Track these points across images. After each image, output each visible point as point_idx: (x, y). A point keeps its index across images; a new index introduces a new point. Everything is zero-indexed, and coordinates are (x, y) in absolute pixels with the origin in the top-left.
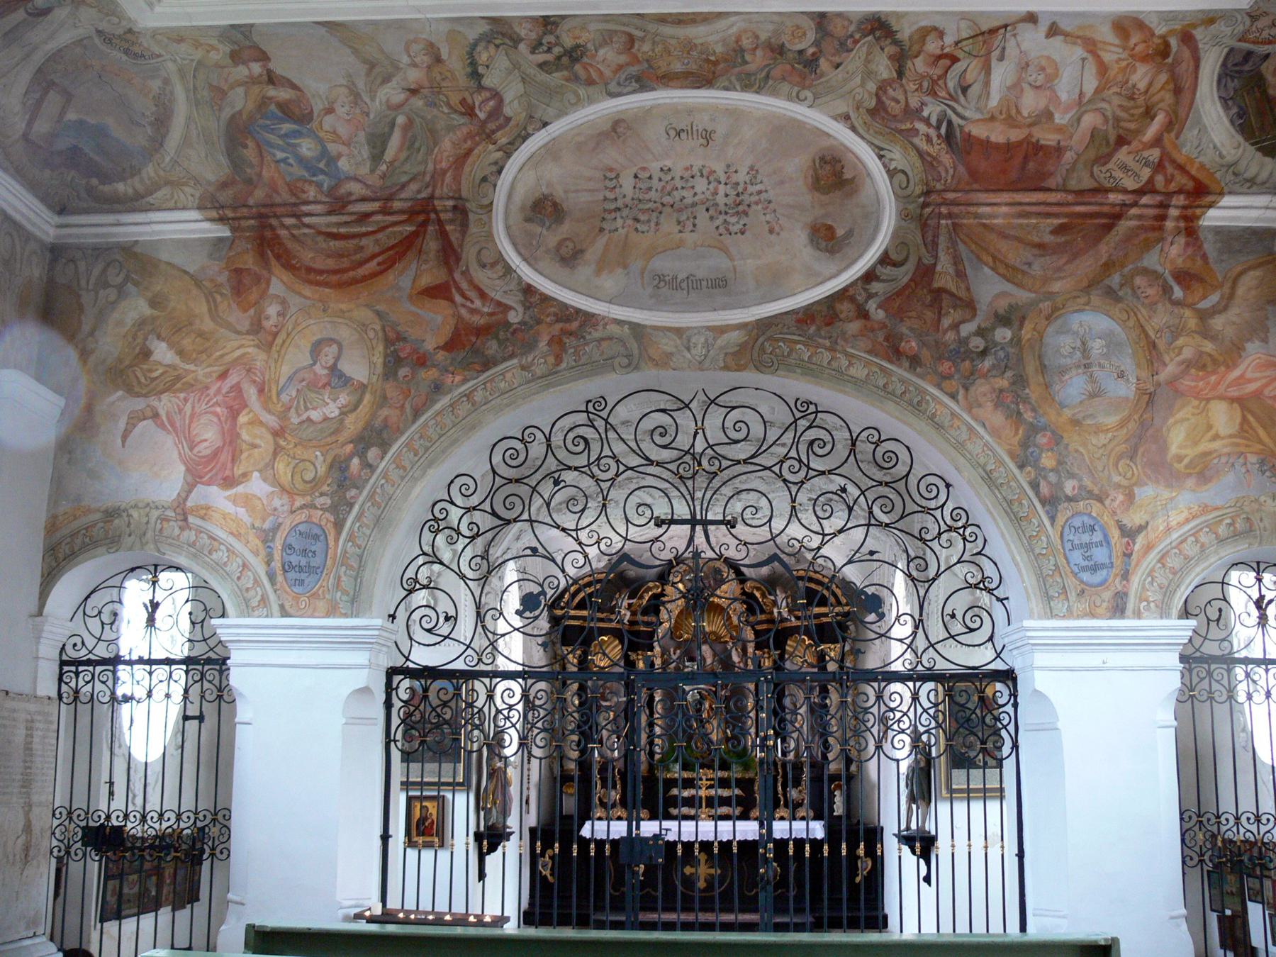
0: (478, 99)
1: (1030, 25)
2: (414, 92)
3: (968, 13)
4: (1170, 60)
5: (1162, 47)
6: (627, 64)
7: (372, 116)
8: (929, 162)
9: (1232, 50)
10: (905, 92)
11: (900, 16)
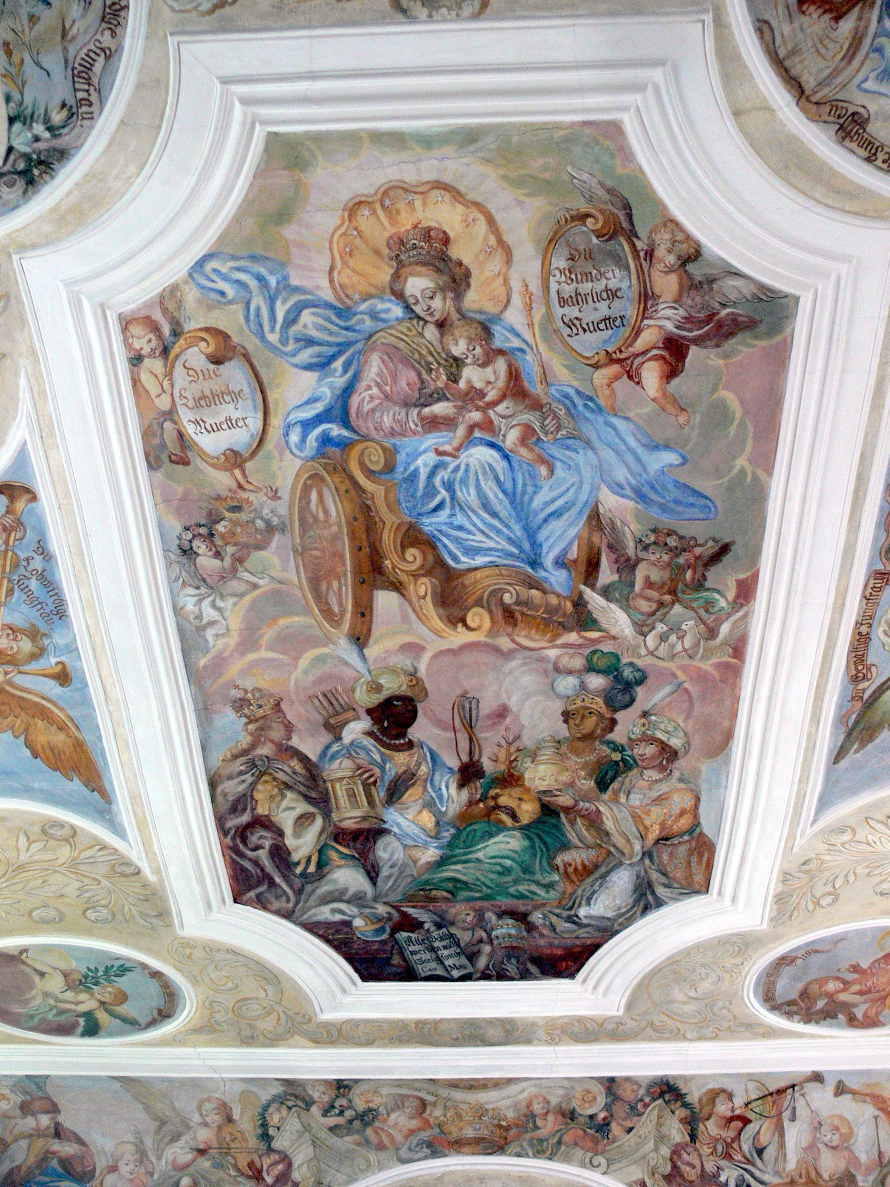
0: (267, 1162)
1: (818, 1085)
2: (202, 1152)
3: (753, 1074)
6: (420, 1129)
7: (156, 1177)
10: (700, 1156)
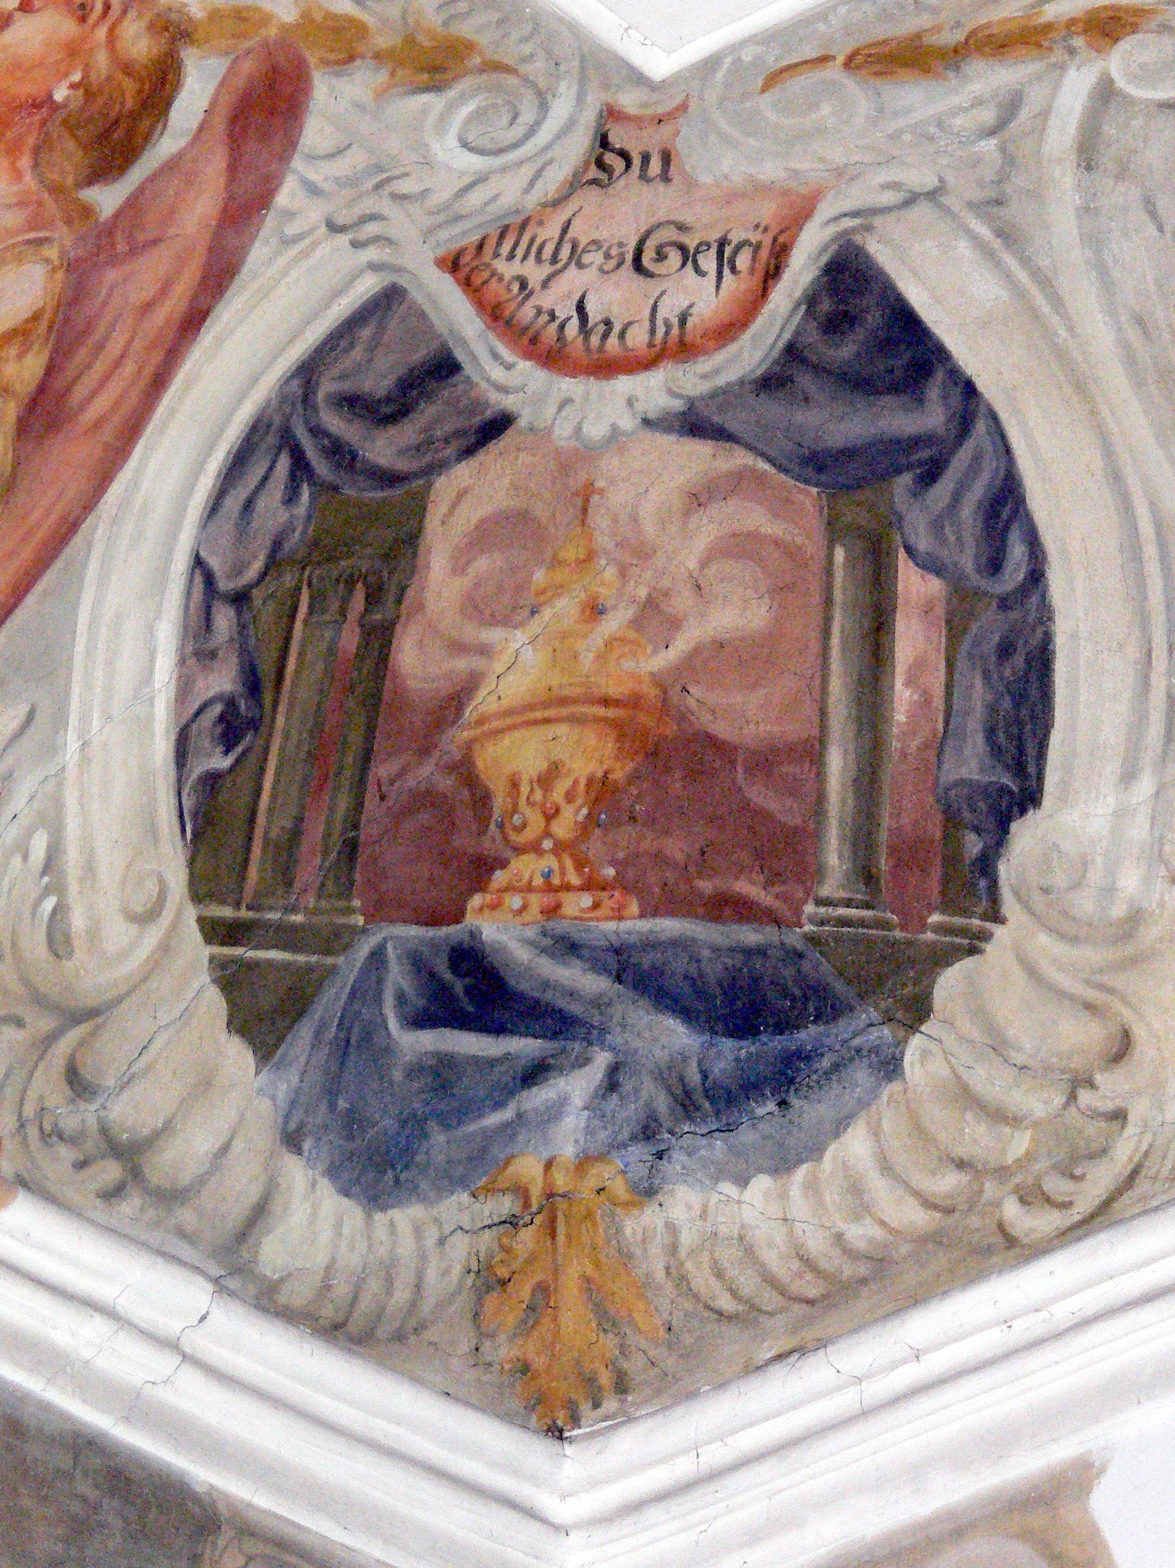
4: (107, 199)
9: (390, 298)
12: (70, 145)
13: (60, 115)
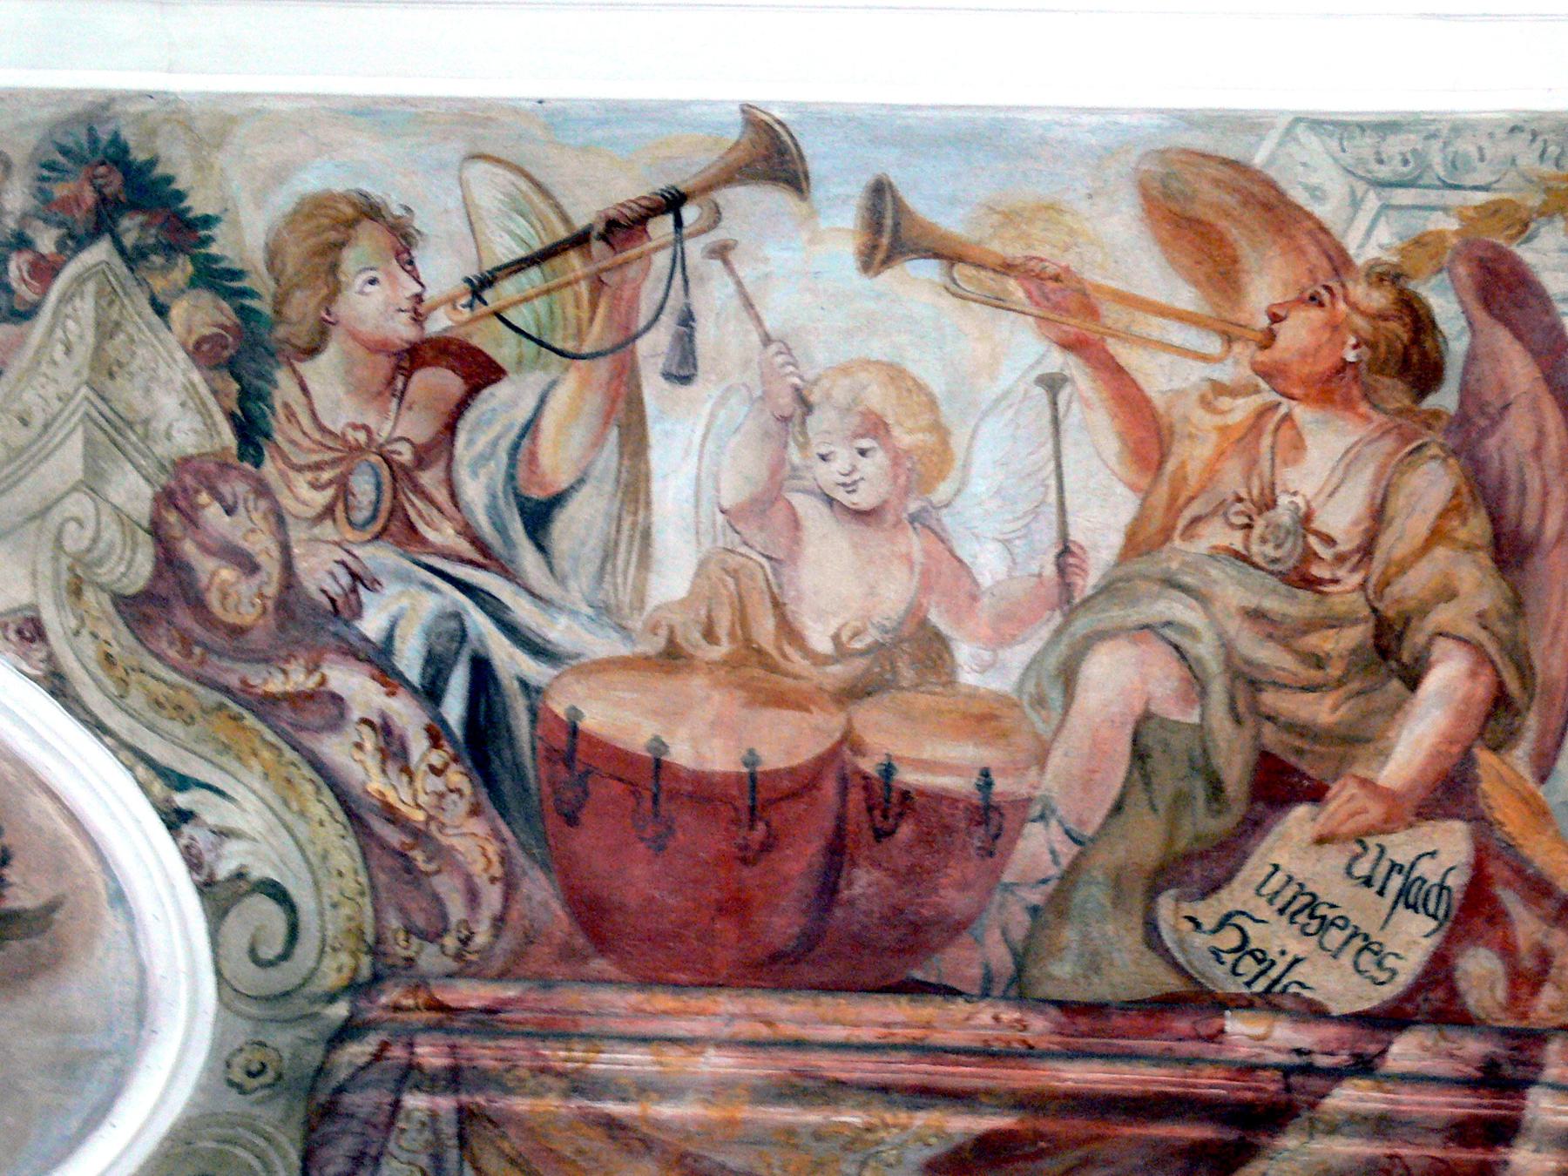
4: (1445, 399)
5: (1398, 330)
8: (391, 849)
10: (279, 519)
11: (214, 125)
12: (1387, 381)
13: (1363, 366)
